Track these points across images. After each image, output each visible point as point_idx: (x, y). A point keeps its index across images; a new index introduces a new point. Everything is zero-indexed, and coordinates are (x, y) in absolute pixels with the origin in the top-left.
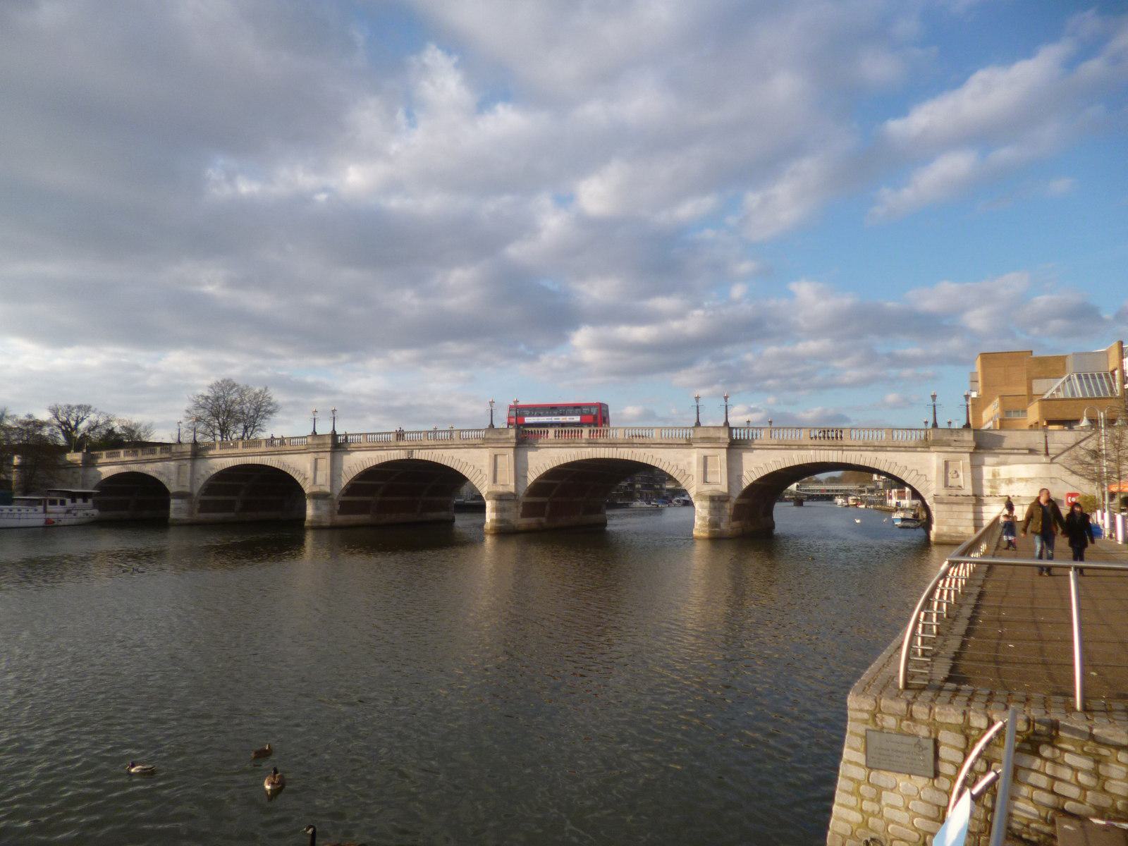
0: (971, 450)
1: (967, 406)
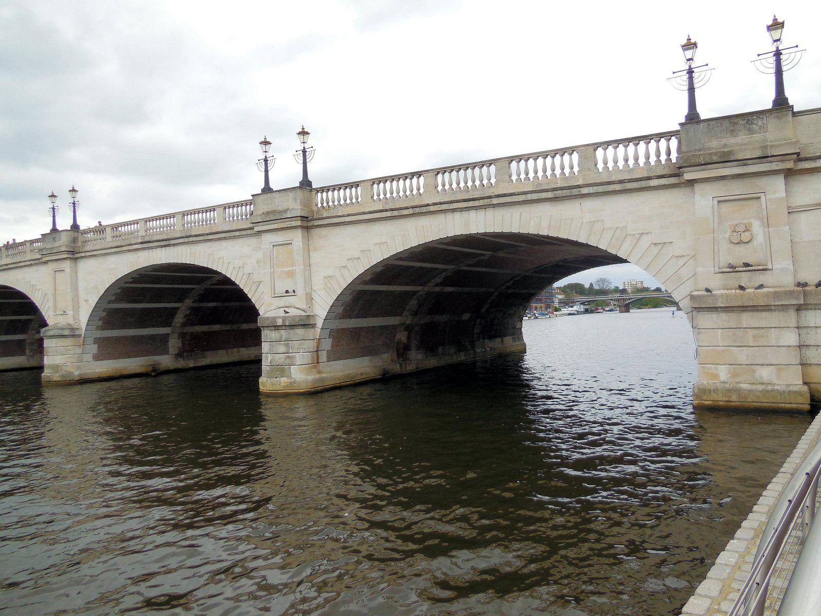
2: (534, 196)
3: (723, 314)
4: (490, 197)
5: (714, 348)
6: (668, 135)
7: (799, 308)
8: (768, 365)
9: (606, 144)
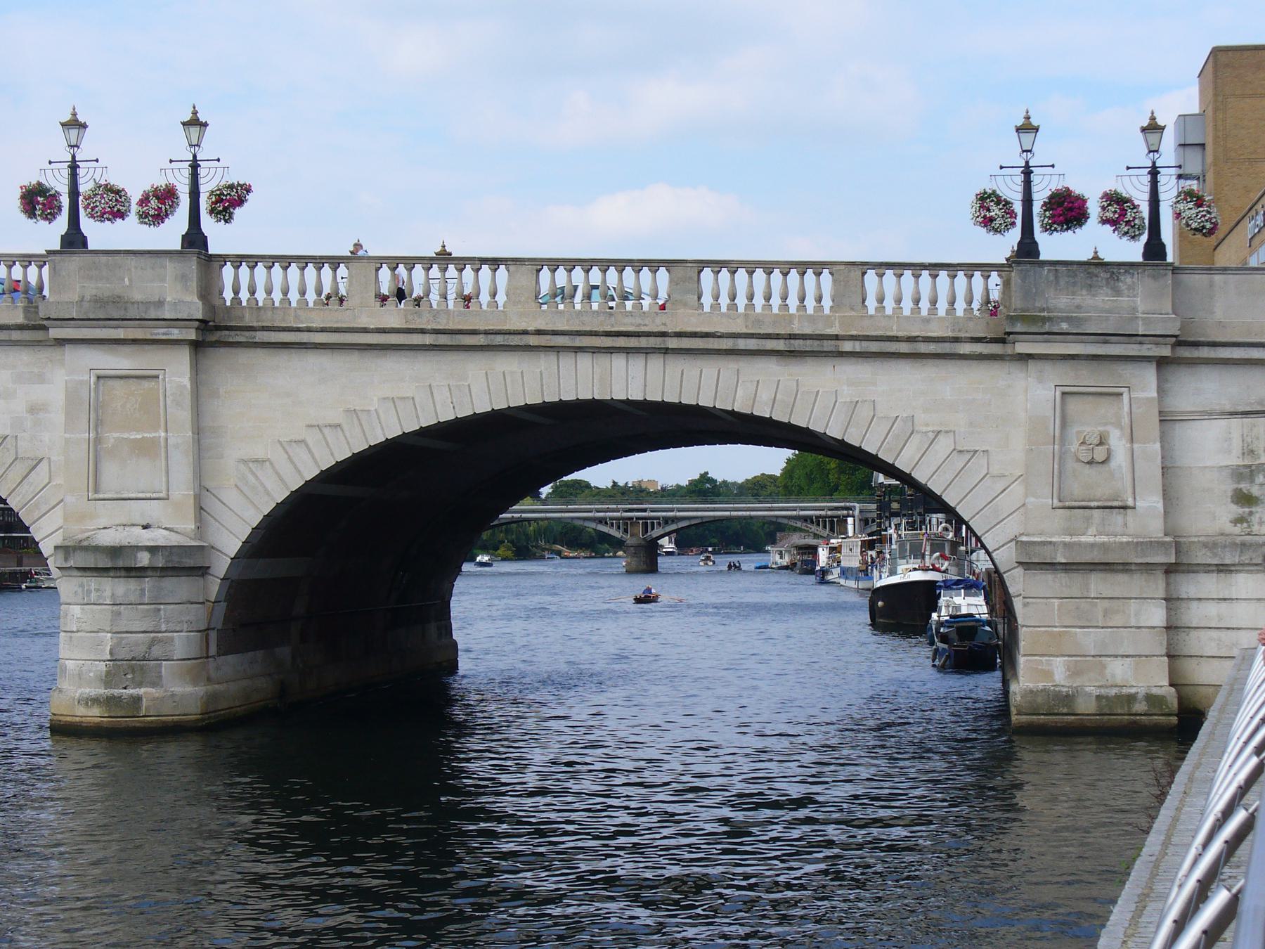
0: (192, 335)
1: (1154, 172)
2: (752, 344)
3: (1063, 575)
4: (663, 334)
5: (1047, 629)
6: (986, 268)
7: (1170, 570)
8: (1123, 656)
9: (881, 267)
